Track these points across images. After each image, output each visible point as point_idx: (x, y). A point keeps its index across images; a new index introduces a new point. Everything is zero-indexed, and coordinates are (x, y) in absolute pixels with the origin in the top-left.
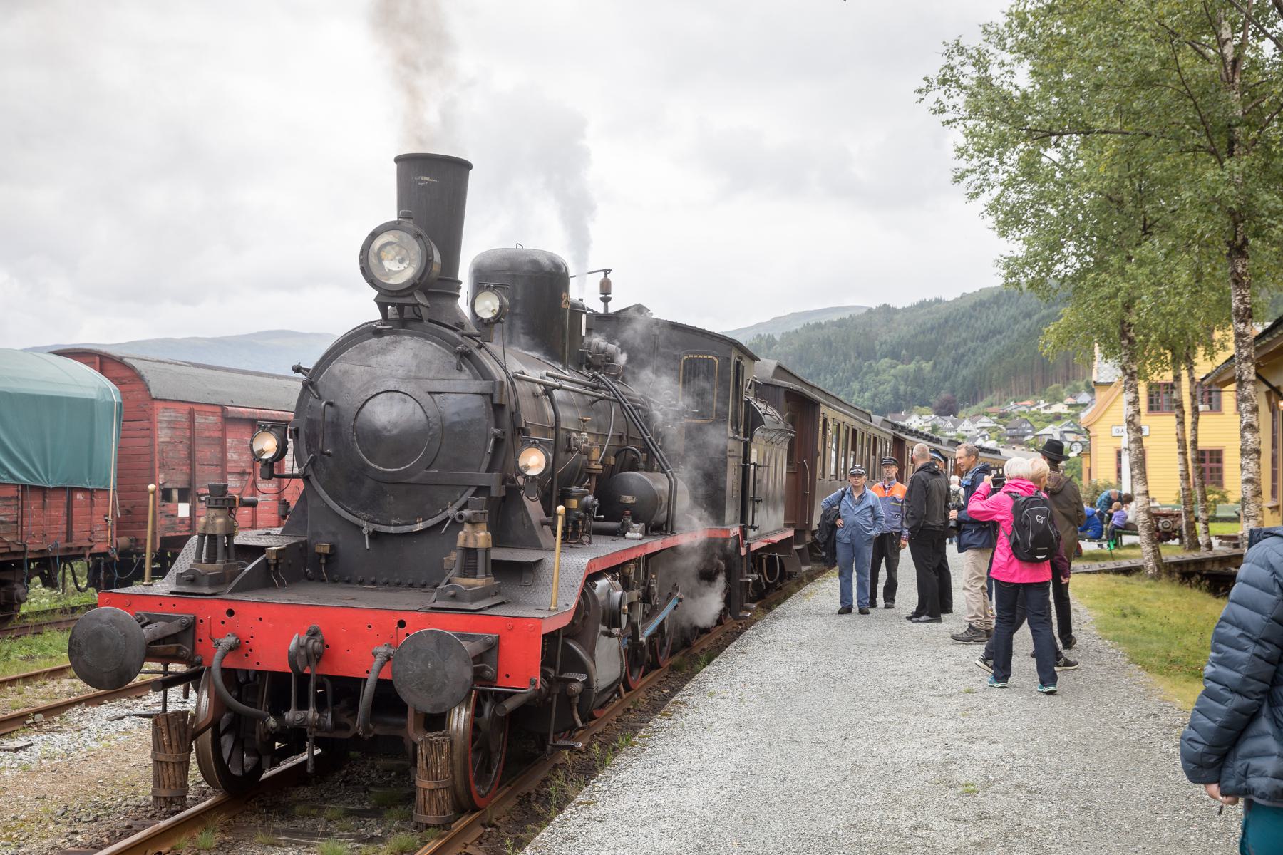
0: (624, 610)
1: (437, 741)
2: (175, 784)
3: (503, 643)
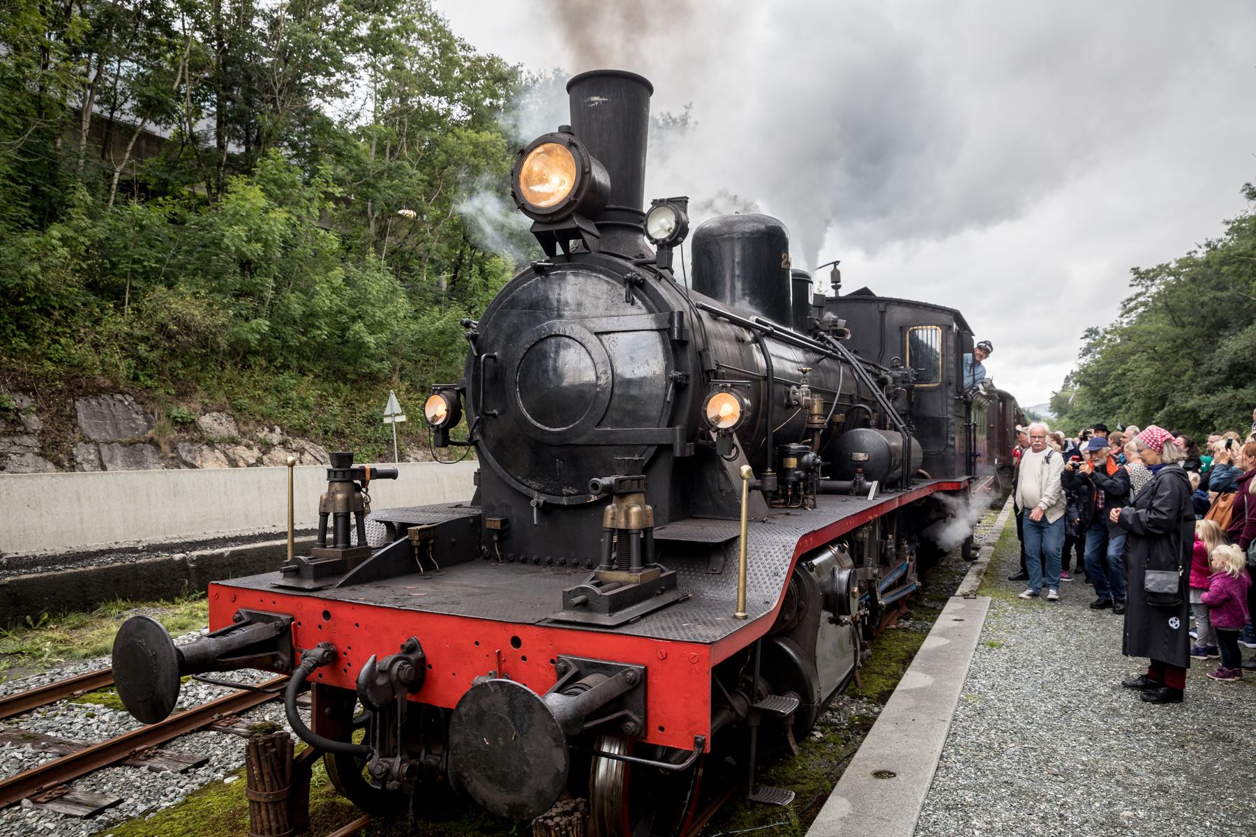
0: (854, 593)
1: (557, 824)
2: (270, 830)
3: (654, 680)
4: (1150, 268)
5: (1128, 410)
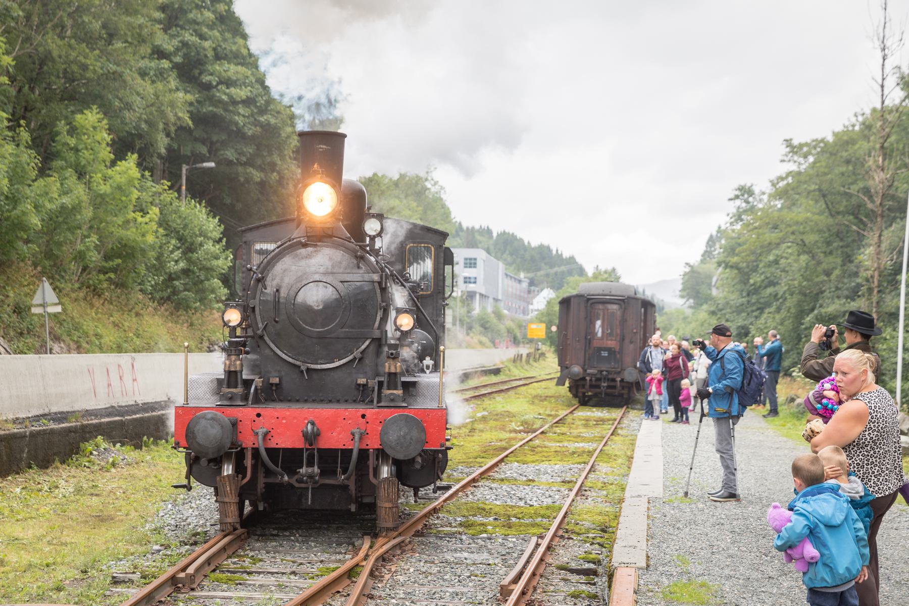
4: (803, 141)
5: (778, 310)
